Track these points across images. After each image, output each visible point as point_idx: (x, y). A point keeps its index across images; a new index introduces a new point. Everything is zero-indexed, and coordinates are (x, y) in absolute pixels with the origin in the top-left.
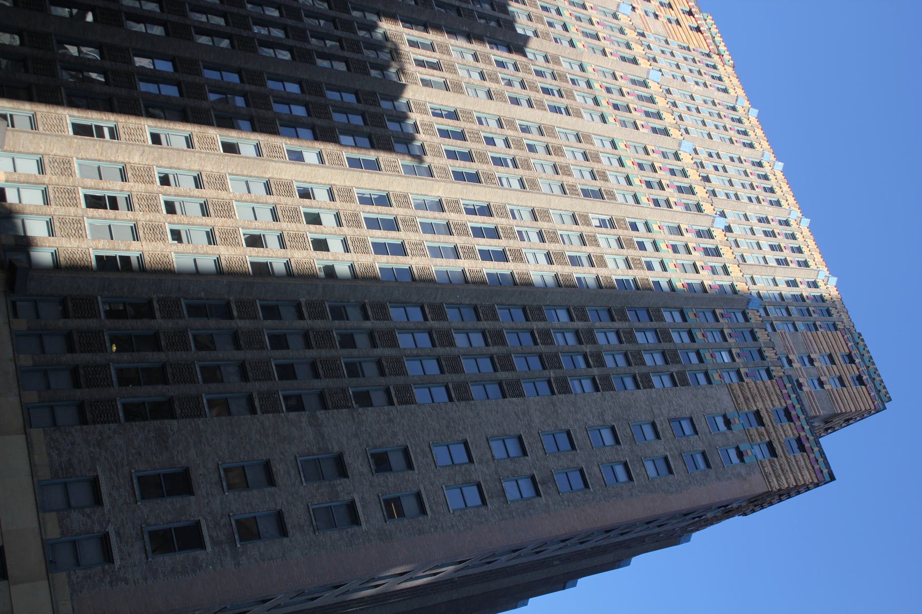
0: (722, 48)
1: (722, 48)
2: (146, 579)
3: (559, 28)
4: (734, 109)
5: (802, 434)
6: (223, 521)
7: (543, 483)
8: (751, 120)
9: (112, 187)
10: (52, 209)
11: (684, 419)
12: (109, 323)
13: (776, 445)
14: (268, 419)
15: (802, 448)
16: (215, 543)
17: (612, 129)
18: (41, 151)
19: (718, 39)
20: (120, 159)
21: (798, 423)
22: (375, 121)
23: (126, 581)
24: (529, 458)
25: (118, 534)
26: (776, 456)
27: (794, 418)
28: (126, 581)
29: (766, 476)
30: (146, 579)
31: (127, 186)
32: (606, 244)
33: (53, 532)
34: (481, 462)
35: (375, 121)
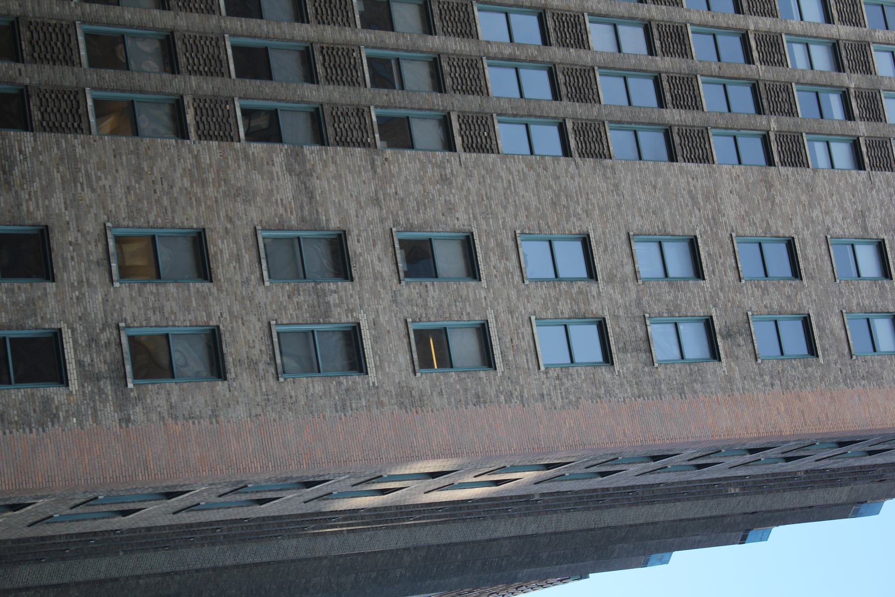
6: (104, 337)
14: (210, 152)
16: (88, 375)
24: (706, 284)
34: (611, 279)
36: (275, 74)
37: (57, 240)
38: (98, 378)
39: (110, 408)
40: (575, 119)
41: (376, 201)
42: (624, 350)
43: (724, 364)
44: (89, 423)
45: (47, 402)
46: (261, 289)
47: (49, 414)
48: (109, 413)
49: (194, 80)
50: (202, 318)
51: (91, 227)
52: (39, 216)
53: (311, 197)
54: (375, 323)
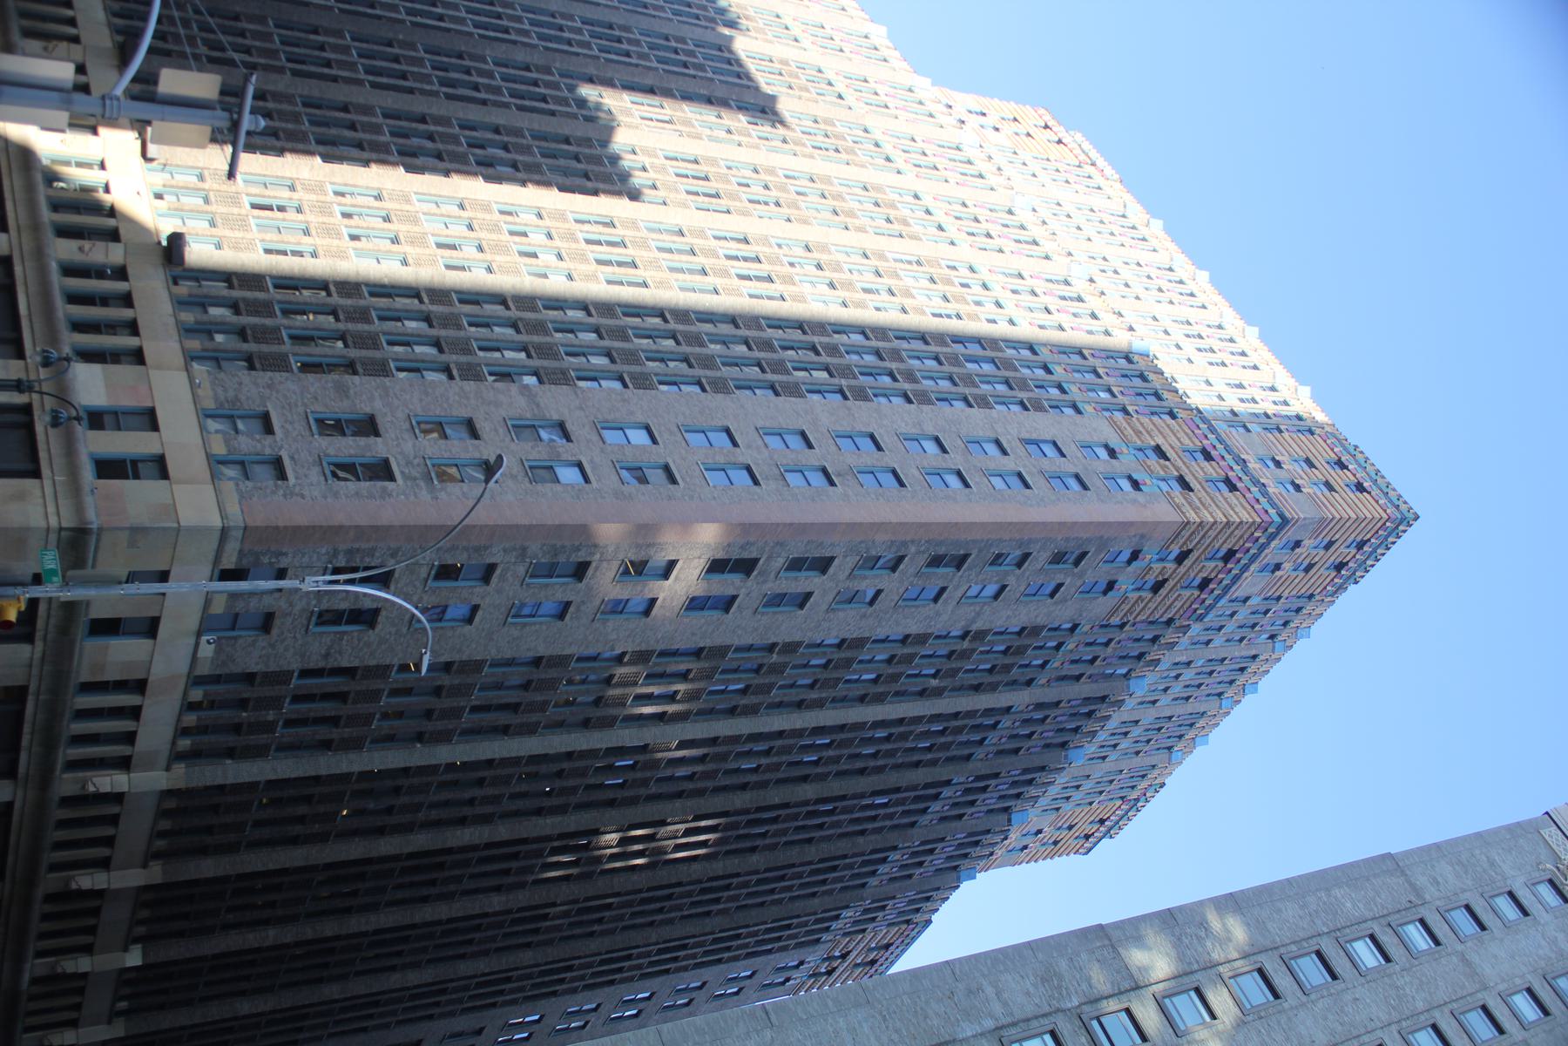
0: (1094, 154)
1: (1094, 154)
2: (325, 497)
3: (977, 289)
4: (1273, 389)
5: (1231, 474)
6: (416, 462)
7: (839, 475)
8: (1250, 338)
9: (281, 195)
10: (213, 208)
11: (1045, 441)
12: (285, 322)
13: (1188, 478)
14: (470, 386)
15: (1233, 488)
16: (406, 477)
17: (910, 181)
18: (200, 165)
19: (1087, 146)
20: (288, 174)
21: (1222, 463)
22: (589, 165)
23: (303, 497)
24: (817, 450)
25: (292, 458)
26: (1167, 459)
27: (1217, 458)
28: (303, 497)
29: (1178, 507)
30: (325, 497)
31: (295, 196)
32: (911, 280)
33: (219, 449)
34: (749, 446)
35: (589, 165)
36: (141, 331)
37: (379, 420)
38: (415, 479)
39: (424, 492)
40: (457, 364)
41: (581, 408)
42: (767, 478)
43: (47, 483)
44: (412, 498)
45: (384, 489)
46: (241, 438)
47: (385, 494)
48: (424, 495)
49: (454, 357)
50: (477, 455)
51: (400, 415)
52: (368, 410)
53: (538, 405)
54: (592, 461)
